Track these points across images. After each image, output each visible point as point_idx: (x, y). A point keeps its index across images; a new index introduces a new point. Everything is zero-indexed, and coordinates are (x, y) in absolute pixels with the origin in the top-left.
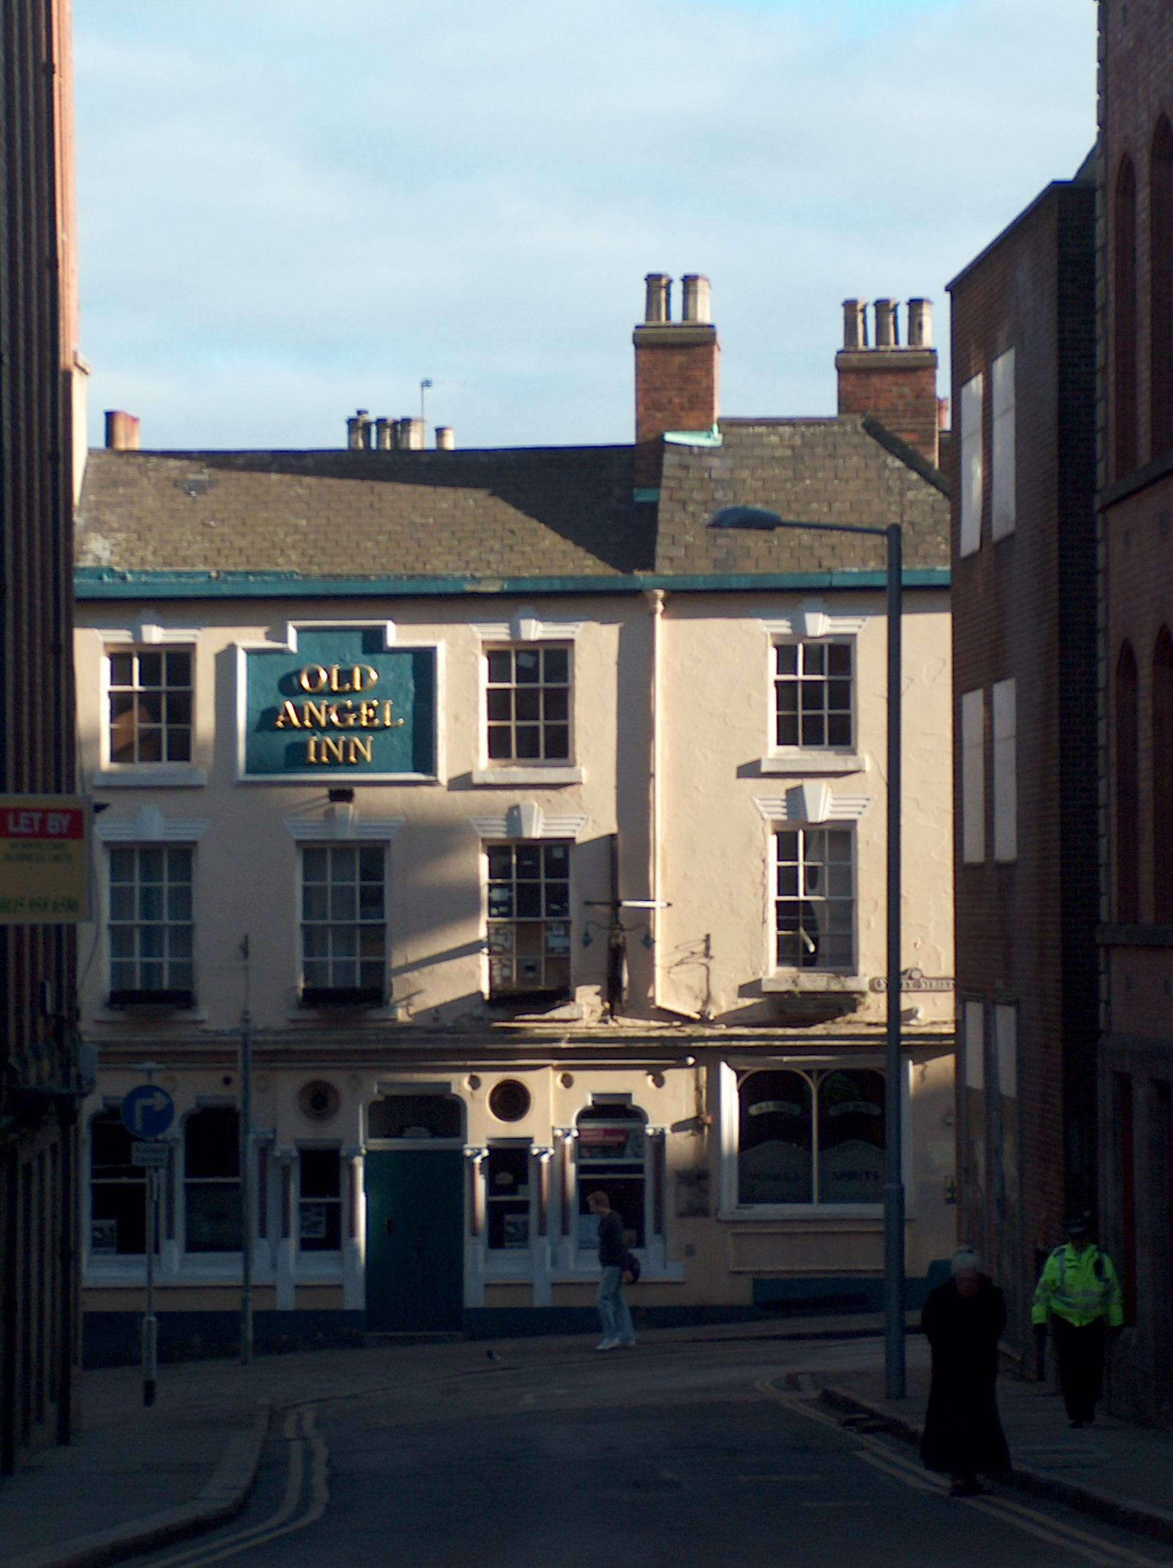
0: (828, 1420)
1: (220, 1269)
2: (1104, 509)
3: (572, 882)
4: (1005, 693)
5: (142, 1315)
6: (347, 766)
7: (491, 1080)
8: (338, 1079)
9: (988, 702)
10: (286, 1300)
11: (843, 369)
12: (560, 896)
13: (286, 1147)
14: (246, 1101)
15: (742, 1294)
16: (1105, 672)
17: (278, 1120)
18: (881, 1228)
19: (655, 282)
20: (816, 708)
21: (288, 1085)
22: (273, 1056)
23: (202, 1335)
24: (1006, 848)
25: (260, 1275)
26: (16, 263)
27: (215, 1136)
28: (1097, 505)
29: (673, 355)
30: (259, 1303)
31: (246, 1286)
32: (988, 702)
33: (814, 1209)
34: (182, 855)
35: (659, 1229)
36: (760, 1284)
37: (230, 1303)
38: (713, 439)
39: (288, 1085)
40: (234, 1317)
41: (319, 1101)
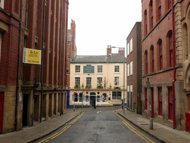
1: (81, 103)
3: (102, 80)
4: (131, 86)
6: (89, 73)
7: (97, 92)
9: (130, 87)
10: (85, 105)
12: (102, 81)
13: (85, 96)
17: (85, 94)
18: (126, 64)
19: (108, 46)
21: (85, 92)
24: (131, 74)
25: (83, 103)
26: (55, 51)
29: (109, 50)
30: (83, 105)
32: (130, 87)
33: (116, 100)
34: (79, 78)
36: (113, 104)
39: (85, 92)
41: (87, 93)
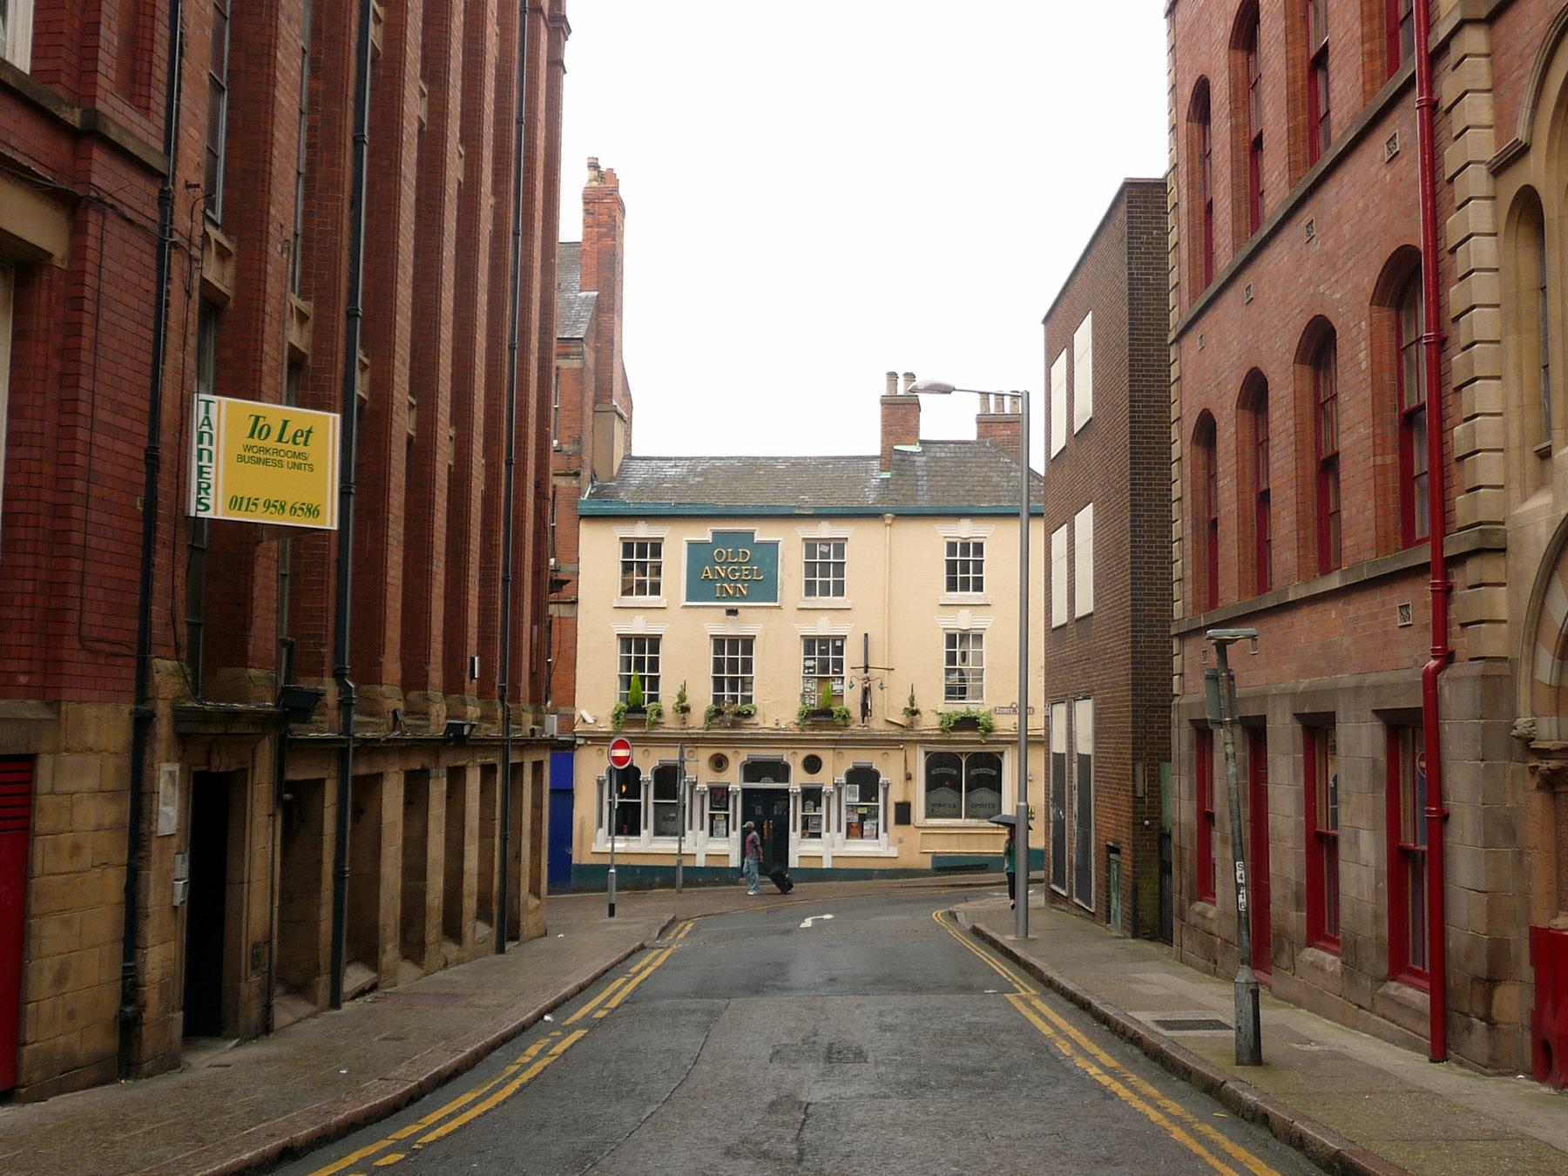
0: (1555, 1063)
1: (667, 845)
2: (1177, 340)
5: (609, 867)
8: (728, 753)
10: (701, 861)
11: (979, 422)
12: (839, 664)
13: (702, 786)
14: (682, 762)
15: (927, 863)
16: (1180, 444)
17: (699, 772)
19: (893, 376)
20: (964, 570)
21: (705, 755)
22: (697, 741)
23: (642, 879)
25: (686, 849)
27: (667, 778)
28: (1172, 336)
29: (900, 411)
30: (687, 863)
31: (680, 854)
34: (655, 642)
35: (885, 830)
36: (936, 858)
37: (672, 862)
38: (916, 448)
39: (705, 755)
40: (673, 869)
41: (719, 763)
